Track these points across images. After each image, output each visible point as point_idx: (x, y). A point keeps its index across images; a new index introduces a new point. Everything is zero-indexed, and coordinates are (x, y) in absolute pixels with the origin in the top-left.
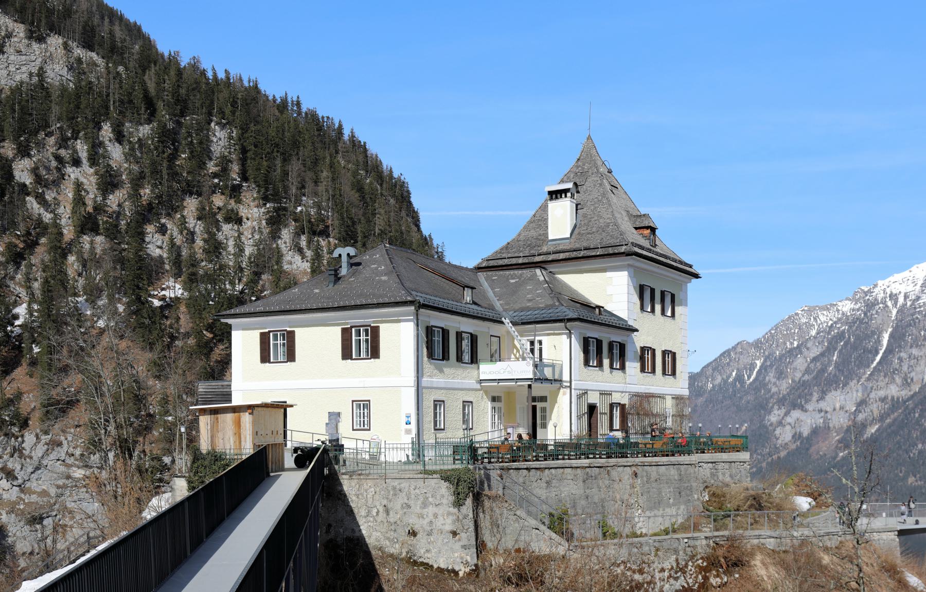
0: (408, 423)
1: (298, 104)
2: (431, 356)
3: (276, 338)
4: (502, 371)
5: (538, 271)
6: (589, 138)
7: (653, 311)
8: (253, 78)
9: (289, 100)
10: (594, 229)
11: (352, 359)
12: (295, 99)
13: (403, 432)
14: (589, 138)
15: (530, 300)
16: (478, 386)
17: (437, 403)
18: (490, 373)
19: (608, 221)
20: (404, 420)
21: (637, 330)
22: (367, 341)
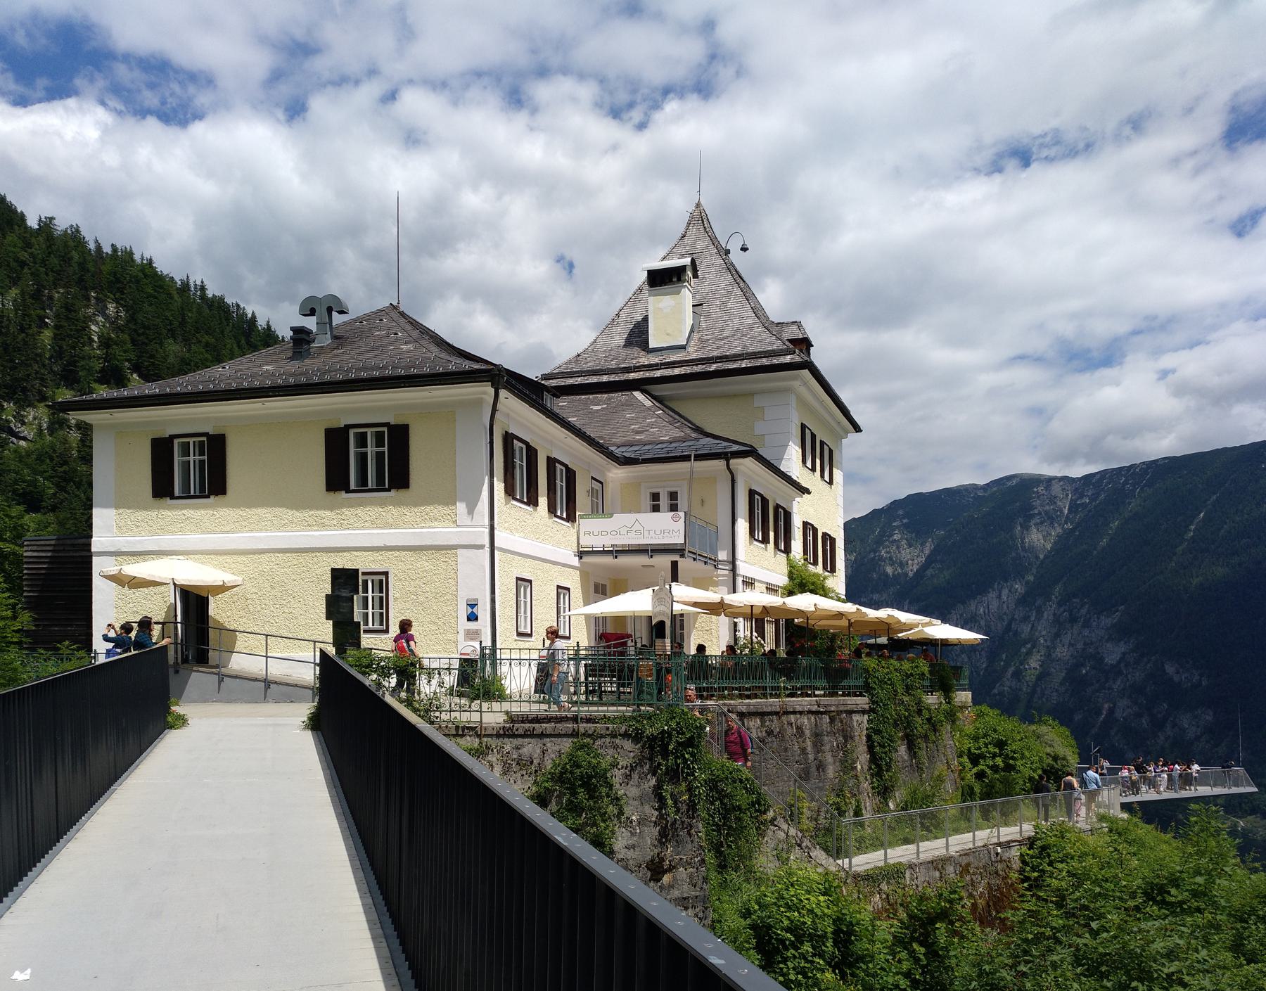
0: (472, 617)
1: (203, 288)
2: (510, 491)
3: (185, 452)
4: (624, 531)
5: (638, 394)
6: (698, 205)
7: (813, 469)
8: (147, 256)
9: (192, 284)
10: (726, 333)
11: (348, 491)
12: (198, 283)
13: (461, 636)
14: (698, 205)
15: (638, 432)
16: (575, 561)
17: (523, 582)
18: (600, 533)
19: (750, 321)
20: (463, 612)
21: (809, 493)
22: (379, 456)
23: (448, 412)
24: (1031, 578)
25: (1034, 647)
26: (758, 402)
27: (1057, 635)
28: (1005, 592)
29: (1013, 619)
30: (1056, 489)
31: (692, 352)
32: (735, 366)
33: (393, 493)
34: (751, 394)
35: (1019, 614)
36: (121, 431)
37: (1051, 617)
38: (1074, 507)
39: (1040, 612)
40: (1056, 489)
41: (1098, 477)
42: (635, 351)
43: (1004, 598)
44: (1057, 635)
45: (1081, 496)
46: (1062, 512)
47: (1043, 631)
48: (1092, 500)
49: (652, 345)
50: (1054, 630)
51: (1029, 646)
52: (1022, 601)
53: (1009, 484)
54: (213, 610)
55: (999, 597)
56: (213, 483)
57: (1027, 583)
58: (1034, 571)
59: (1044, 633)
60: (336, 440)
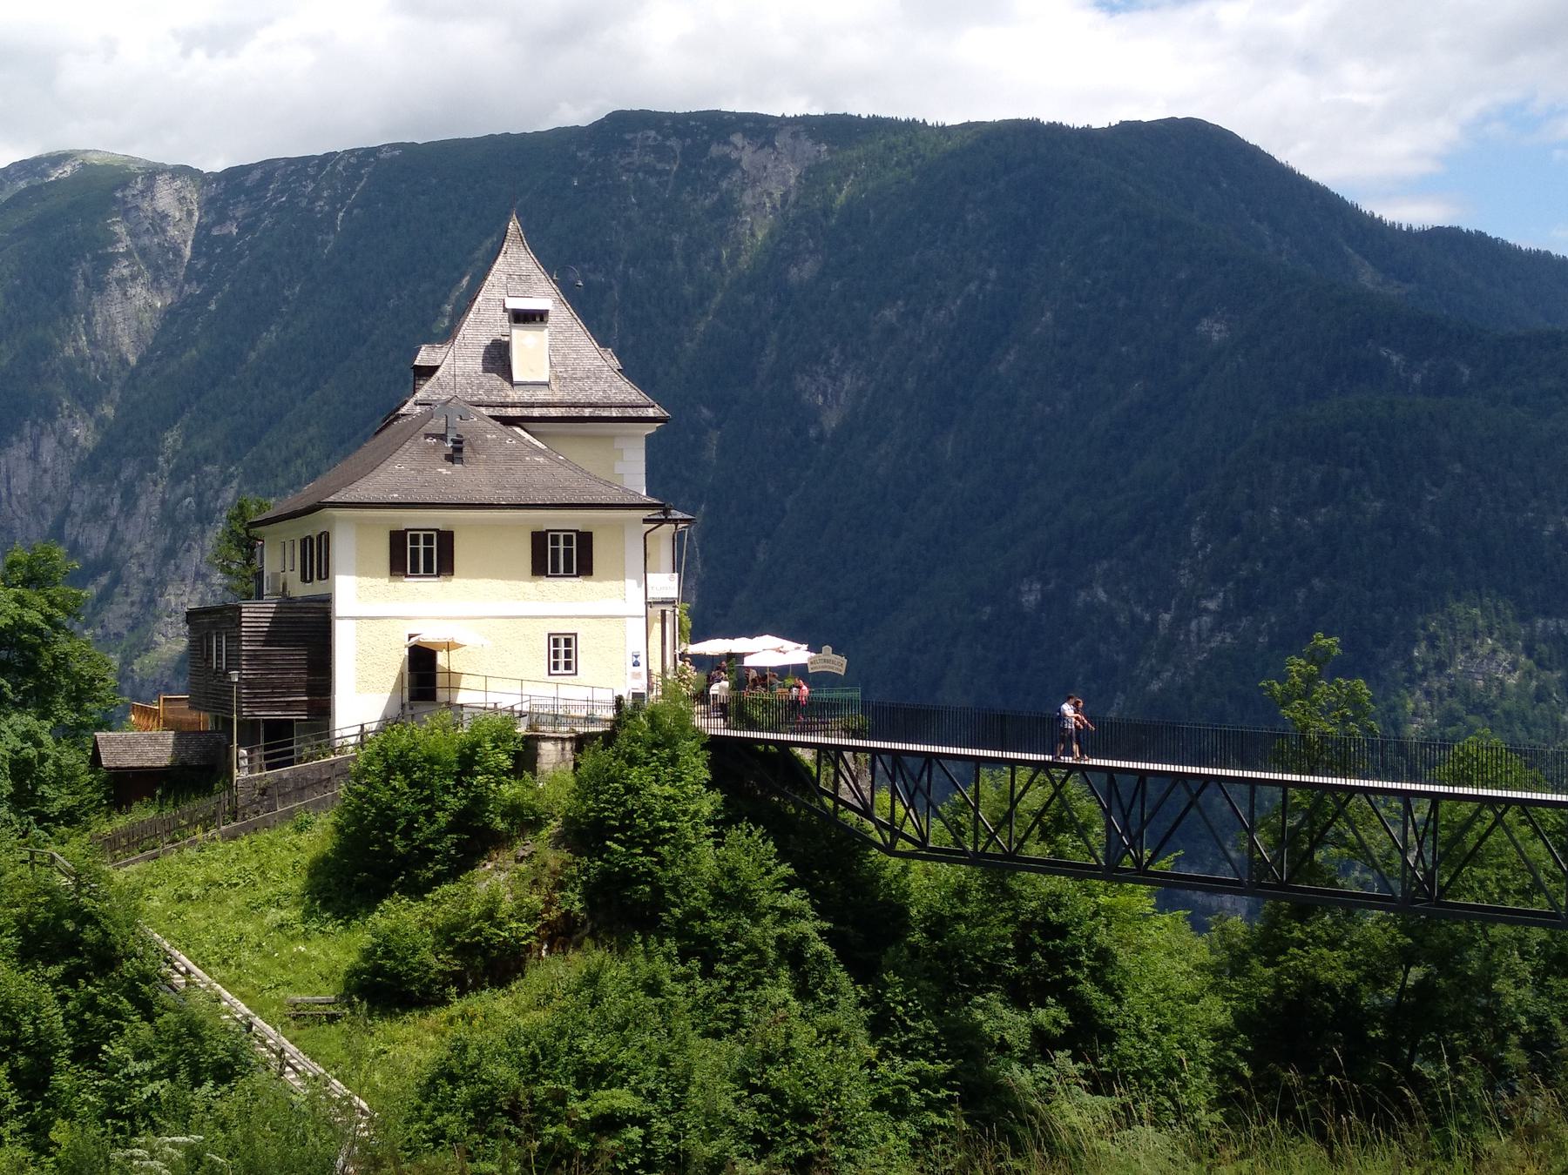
0: (636, 664)
5: (518, 430)
23: (621, 526)
24: (109, 411)
25: (116, 581)
26: (618, 444)
27: (169, 553)
28: (48, 445)
29: (67, 512)
30: (165, 198)
31: (557, 395)
32: (606, 414)
33: (580, 579)
34: (613, 437)
35: (81, 501)
36: (361, 524)
37: (156, 509)
38: (203, 239)
39: (130, 498)
40: (165, 198)
41: (257, 175)
42: (495, 380)
43: (46, 458)
44: (169, 553)
45: (221, 220)
46: (178, 253)
47: (140, 540)
48: (243, 230)
49: (516, 379)
50: (163, 542)
51: (104, 580)
52: (91, 466)
53: (55, 175)
54: (441, 659)
55: (34, 457)
56: (445, 567)
57: (100, 422)
58: (116, 394)
59: (139, 547)
60: (539, 541)
